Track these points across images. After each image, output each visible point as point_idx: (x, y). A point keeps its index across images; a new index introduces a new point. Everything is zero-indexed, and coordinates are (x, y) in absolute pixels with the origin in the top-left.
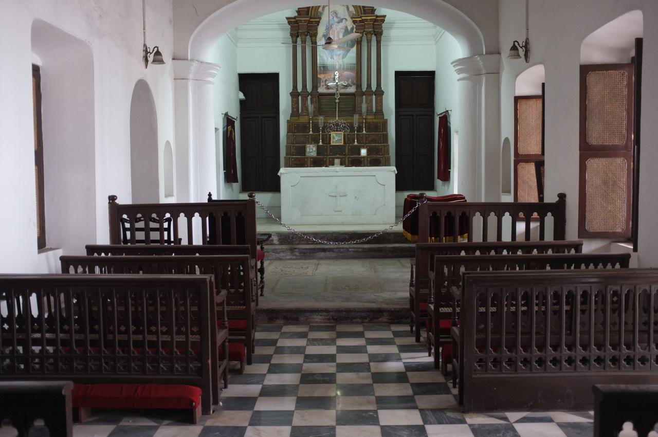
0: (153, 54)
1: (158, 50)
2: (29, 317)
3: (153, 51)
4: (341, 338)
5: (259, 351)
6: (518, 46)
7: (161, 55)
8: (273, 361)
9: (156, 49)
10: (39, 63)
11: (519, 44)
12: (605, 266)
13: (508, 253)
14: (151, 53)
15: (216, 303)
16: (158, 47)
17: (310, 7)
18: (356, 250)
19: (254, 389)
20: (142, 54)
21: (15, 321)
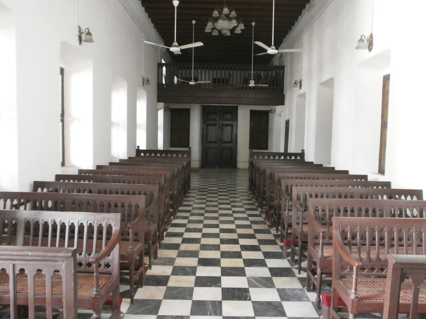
0: (85, 34)
1: (89, 30)
2: (126, 169)
3: (85, 31)
4: (202, 150)
5: (162, 253)
6: (364, 39)
7: (91, 36)
8: (192, 212)
9: (87, 30)
10: (63, 66)
11: (365, 38)
12: (406, 197)
13: (412, 199)
14: (83, 33)
15: (271, 111)
16: (88, 29)
17: (194, 42)
18: (254, 179)
19: (167, 270)
20: (78, 33)
21: (58, 182)
